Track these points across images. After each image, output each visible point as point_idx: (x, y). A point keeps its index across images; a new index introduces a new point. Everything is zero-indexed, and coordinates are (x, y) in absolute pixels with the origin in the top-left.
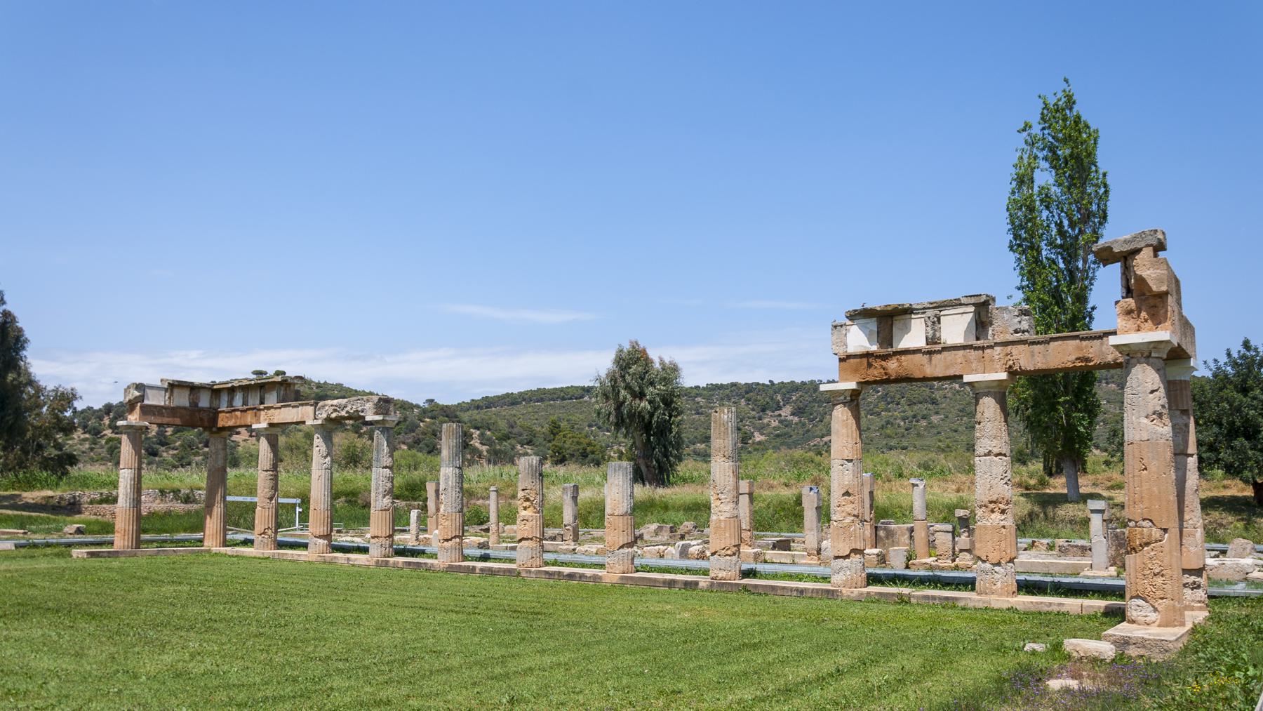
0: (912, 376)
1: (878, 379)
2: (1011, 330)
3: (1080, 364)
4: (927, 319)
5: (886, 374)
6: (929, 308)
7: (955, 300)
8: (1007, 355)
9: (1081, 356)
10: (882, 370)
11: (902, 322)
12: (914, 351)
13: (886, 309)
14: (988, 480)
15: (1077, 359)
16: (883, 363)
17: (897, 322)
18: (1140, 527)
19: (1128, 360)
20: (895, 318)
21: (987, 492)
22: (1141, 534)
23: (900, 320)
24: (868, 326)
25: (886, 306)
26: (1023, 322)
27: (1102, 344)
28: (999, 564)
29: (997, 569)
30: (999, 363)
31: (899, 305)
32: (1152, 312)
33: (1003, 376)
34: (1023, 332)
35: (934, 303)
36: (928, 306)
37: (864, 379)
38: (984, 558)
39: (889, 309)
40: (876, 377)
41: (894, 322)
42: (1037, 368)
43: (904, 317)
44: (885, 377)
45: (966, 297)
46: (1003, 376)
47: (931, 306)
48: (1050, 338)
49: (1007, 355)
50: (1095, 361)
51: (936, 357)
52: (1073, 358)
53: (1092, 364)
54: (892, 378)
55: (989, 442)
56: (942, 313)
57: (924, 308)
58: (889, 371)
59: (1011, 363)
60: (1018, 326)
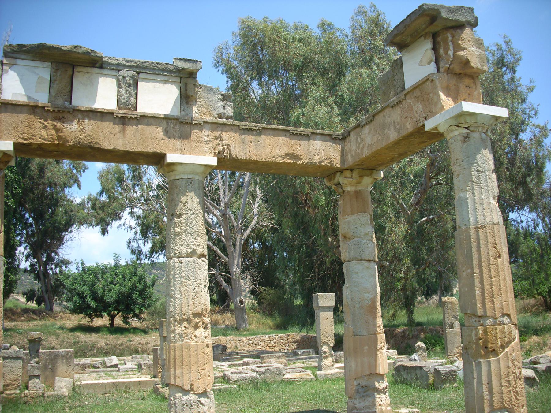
0: (98, 146)
1: (47, 142)
2: (215, 113)
3: (289, 161)
4: (121, 78)
5: (59, 138)
6: (124, 66)
7: (158, 63)
8: (216, 138)
9: (291, 152)
10: (54, 132)
11: (87, 76)
12: (102, 113)
13: (74, 50)
14: (192, 287)
15: (287, 155)
16: (59, 124)
17: (79, 72)
18: (500, 324)
19: (468, 134)
20: (77, 69)
21: (191, 302)
22: (503, 332)
23: (84, 72)
24: (37, 71)
25: (76, 47)
26: (228, 108)
27: (309, 144)
28: (204, 394)
29: (203, 400)
30: (208, 146)
31: (92, 51)
32: (468, 92)
33: (214, 161)
34: (227, 118)
35: (131, 61)
36: (124, 63)
37: (26, 140)
38: (187, 387)
39: (80, 51)
40: (45, 140)
41: (76, 73)
42: (248, 158)
43: (89, 70)
44: (57, 142)
45: (180, 59)
46: (214, 161)
47: (127, 64)
48: (263, 128)
49: (216, 138)
50: (304, 160)
51: (130, 129)
52: (282, 152)
53: (300, 162)
54: (68, 144)
55: (193, 240)
56: (141, 75)
57: (118, 64)
58: (66, 135)
59: (220, 148)
60: (222, 111)
